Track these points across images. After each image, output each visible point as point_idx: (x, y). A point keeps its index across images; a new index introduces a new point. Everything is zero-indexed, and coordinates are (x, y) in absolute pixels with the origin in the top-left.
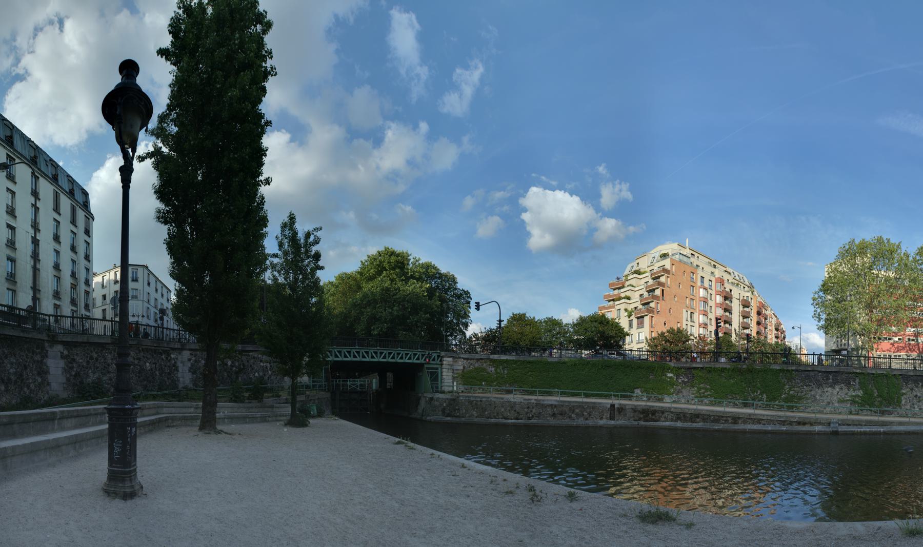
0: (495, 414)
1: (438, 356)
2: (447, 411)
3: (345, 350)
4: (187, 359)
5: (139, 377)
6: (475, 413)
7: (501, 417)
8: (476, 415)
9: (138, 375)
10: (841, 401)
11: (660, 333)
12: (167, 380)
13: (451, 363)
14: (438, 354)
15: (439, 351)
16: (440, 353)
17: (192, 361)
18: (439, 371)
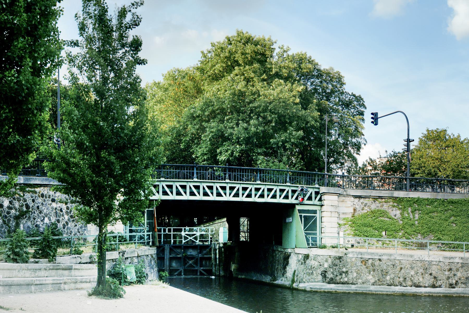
0: (401, 279)
2: (330, 275)
8: (372, 281)
14: (317, 190)
18: (318, 215)
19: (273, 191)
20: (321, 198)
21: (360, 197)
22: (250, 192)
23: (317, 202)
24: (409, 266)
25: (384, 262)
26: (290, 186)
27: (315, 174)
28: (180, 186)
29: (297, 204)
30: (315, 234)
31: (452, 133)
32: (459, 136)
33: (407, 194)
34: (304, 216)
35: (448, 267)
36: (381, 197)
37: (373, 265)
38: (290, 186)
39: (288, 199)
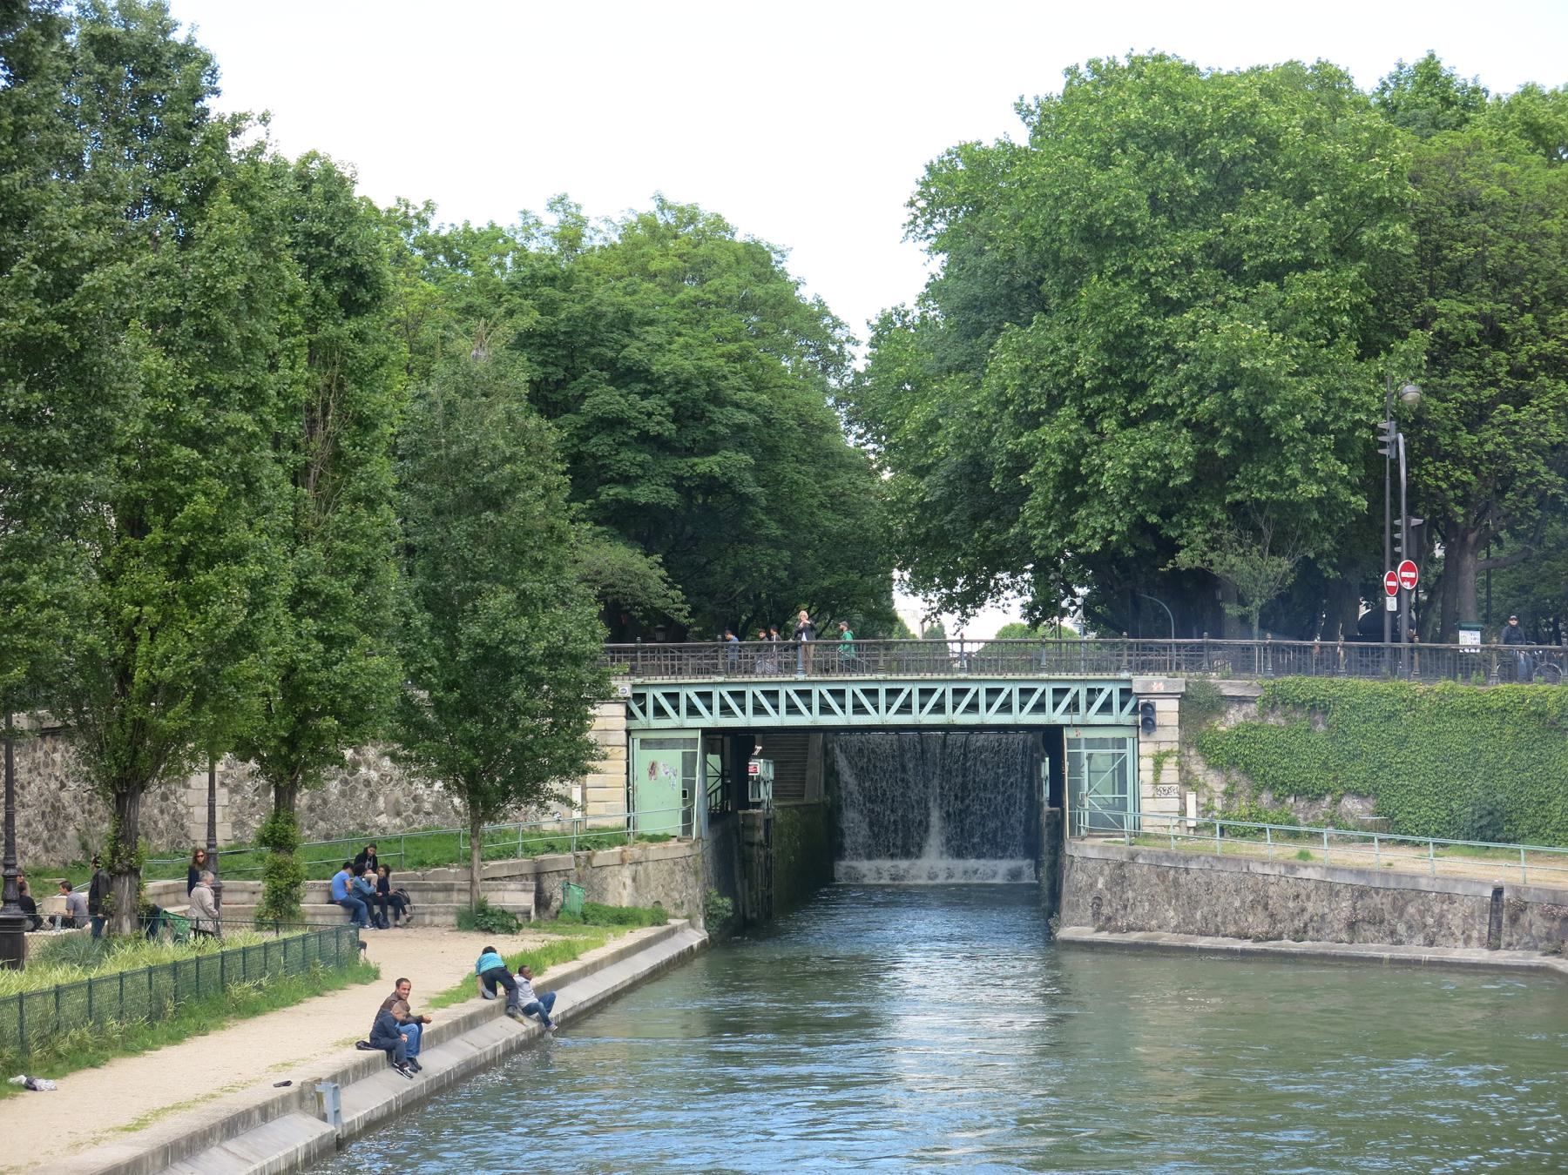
1: (1122, 691)
3: (691, 692)
5: (90, 813)
6: (1172, 913)
7: (1232, 929)
8: (1173, 923)
9: (87, 807)
10: (1400, 97)
11: (875, 322)
12: (159, 816)
15: (1125, 675)
16: (1129, 681)
19: (902, 697)
22: (1091, 699)
26: (1048, 681)
28: (763, 692)
29: (1068, 726)
31: (399, 200)
32: (467, 223)
37: (1176, 883)
38: (1048, 681)
39: (911, 713)
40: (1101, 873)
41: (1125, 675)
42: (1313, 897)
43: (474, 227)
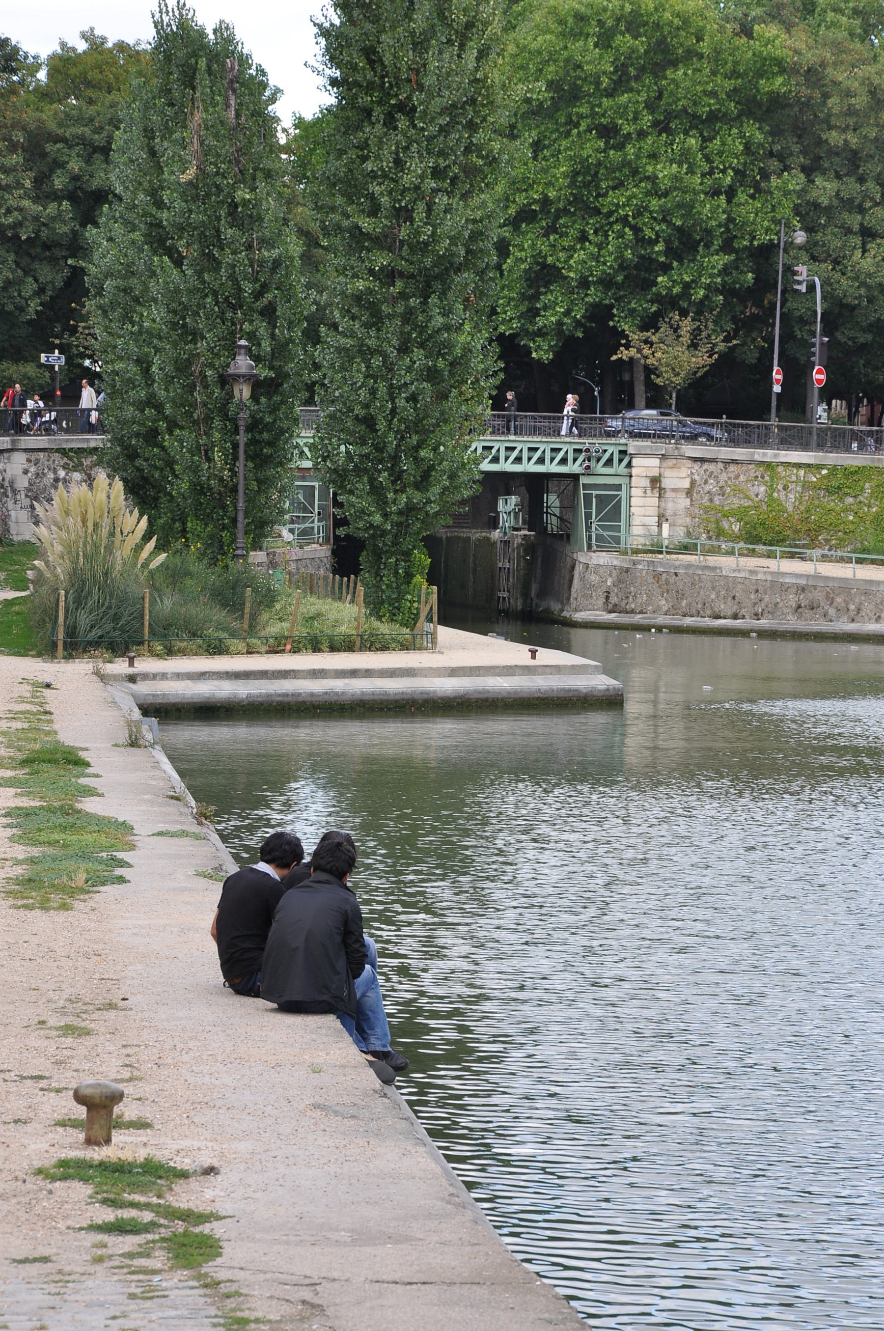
0: (700, 606)
1: (621, 452)
2: (614, 600)
4: (20, 472)
6: (664, 602)
7: (709, 612)
8: (665, 608)
13: (655, 473)
14: (622, 448)
15: (623, 441)
17: (30, 475)
18: (623, 494)
20: (630, 462)
21: (702, 460)
23: (622, 469)
24: (709, 585)
25: (680, 577)
27: (595, 419)
30: (618, 529)
33: (776, 456)
34: (597, 496)
35: (755, 587)
36: (734, 462)
37: (667, 583)
40: (610, 575)
41: (623, 441)
42: (769, 592)
43: (308, 117)
